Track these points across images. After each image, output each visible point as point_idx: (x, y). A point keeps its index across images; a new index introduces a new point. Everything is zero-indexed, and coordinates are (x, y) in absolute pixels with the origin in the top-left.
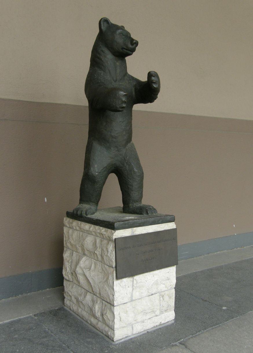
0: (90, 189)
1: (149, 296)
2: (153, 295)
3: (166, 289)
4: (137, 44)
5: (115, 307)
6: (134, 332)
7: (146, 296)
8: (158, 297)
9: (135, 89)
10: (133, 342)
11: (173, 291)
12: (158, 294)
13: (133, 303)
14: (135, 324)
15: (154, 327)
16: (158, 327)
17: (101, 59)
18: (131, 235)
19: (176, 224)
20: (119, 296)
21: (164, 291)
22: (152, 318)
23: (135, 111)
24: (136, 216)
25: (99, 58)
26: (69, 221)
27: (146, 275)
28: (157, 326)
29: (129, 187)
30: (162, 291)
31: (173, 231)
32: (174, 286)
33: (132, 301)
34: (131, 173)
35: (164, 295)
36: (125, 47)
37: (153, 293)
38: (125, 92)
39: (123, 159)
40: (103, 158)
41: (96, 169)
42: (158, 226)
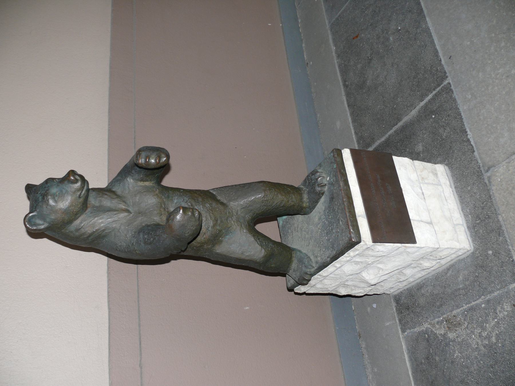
0: (277, 263)
4: (72, 172)
5: (441, 247)
6: (461, 222)
9: (142, 180)
11: (417, 163)
12: (422, 185)
15: (454, 195)
16: (454, 189)
17: (90, 235)
19: (343, 149)
25: (89, 236)
28: (453, 191)
29: (282, 205)
31: (355, 154)
32: (411, 160)
34: (266, 201)
36: (79, 193)
38: (180, 211)
39: (243, 210)
40: (240, 243)
41: (255, 251)
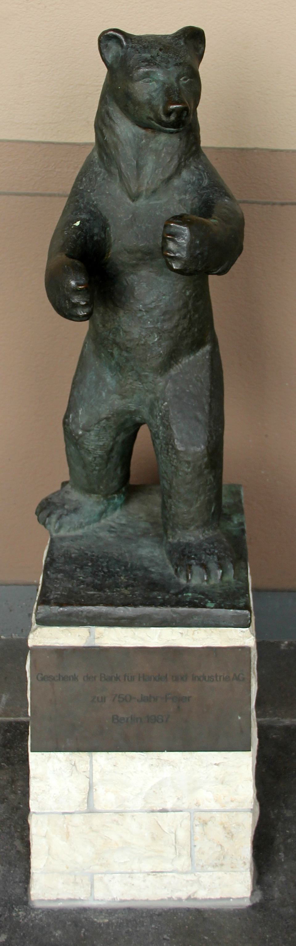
1: (153, 811)
2: (168, 813)
3: (217, 807)
7: (141, 811)
8: (187, 822)
10: (76, 923)
12: (186, 814)
13: (96, 820)
14: (103, 875)
18: (86, 645)
20: (44, 791)
21: (211, 811)
22: (162, 874)
23: (204, 147)
24: (40, 643)
26: (152, 92)
27: (133, 758)
30: (202, 807)
33: (91, 811)
35: (209, 823)
37: (169, 806)
42: (188, 630)
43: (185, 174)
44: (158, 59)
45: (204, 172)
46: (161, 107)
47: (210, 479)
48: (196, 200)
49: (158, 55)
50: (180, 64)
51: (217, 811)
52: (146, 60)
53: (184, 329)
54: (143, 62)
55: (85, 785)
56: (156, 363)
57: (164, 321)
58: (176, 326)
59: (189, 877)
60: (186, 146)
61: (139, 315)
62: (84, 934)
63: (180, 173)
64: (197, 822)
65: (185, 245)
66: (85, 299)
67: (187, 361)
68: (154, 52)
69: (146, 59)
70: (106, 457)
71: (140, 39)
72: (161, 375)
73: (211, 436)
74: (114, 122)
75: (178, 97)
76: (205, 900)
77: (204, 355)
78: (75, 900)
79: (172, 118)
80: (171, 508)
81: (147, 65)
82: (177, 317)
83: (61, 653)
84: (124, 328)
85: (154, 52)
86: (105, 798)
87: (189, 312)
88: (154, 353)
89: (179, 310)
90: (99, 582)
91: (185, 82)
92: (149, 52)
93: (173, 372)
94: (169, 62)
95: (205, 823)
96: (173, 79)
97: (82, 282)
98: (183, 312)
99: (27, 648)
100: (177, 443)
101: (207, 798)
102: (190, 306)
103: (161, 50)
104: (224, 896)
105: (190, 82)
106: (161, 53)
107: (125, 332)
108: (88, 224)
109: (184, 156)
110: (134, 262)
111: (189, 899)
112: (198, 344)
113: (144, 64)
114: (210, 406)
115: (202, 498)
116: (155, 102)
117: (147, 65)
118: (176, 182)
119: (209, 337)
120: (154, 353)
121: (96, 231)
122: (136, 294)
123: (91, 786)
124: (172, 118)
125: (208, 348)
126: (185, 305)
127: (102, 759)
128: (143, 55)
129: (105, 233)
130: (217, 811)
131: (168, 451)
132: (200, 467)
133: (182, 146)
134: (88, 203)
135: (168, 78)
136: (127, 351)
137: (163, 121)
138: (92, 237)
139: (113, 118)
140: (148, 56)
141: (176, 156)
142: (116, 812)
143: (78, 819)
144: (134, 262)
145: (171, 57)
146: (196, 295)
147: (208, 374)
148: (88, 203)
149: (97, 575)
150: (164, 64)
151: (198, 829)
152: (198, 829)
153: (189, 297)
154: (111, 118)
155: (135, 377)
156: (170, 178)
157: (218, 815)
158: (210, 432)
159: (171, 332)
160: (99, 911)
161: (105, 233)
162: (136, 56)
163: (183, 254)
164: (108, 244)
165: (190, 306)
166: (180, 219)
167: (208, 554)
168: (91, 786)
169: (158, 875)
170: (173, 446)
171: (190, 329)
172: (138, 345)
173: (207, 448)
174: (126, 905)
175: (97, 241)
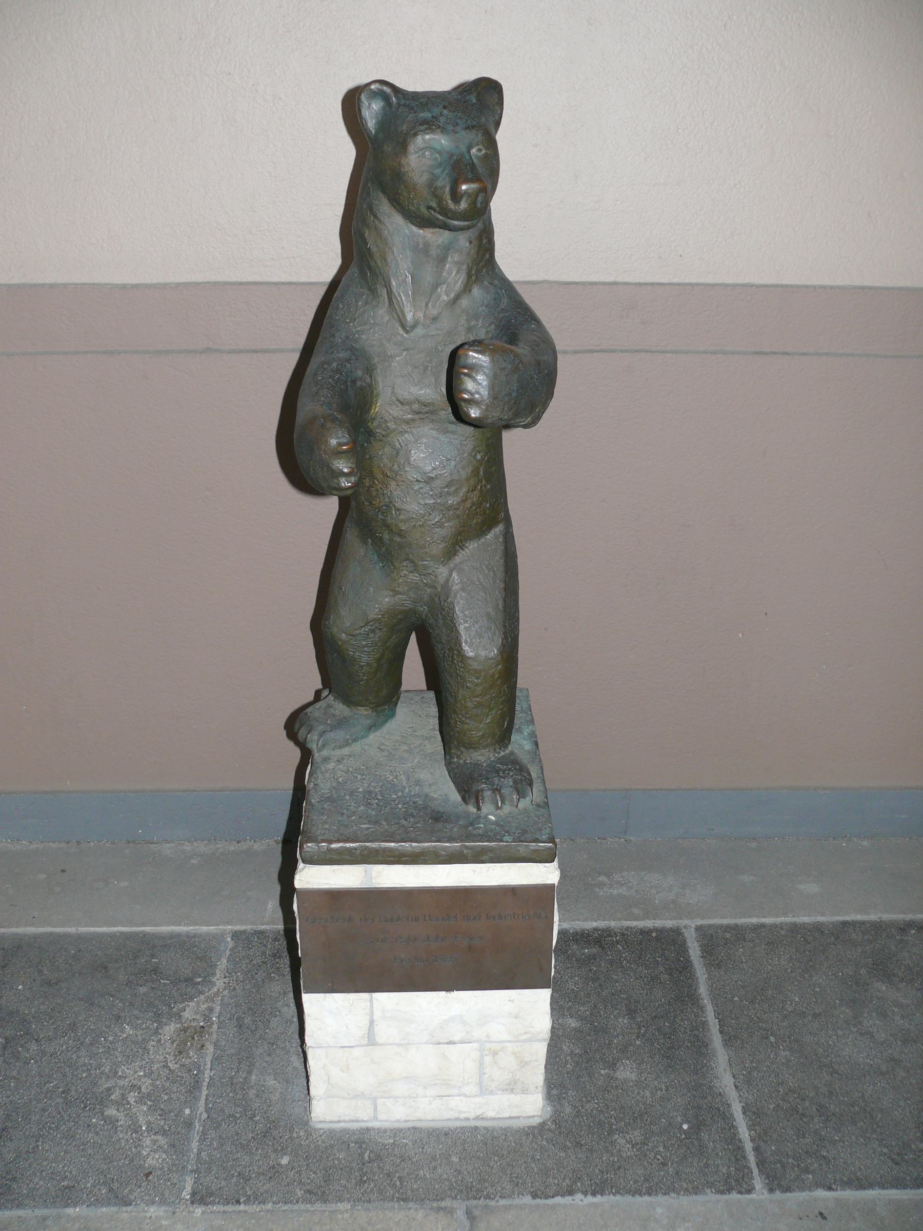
1: (439, 1044)
7: (426, 1043)
12: (476, 1045)
21: (502, 1042)
43: (476, 291)
44: (442, 119)
45: (501, 289)
46: (448, 189)
47: (504, 691)
48: (493, 327)
49: (442, 115)
50: (473, 127)
51: (509, 1041)
52: (424, 122)
53: (473, 504)
54: (420, 124)
55: (365, 1022)
56: (437, 549)
57: (448, 493)
58: (464, 501)
59: (478, 1100)
60: (478, 252)
61: (416, 488)
62: (369, 1156)
63: (470, 291)
64: (487, 1053)
65: (485, 383)
66: (350, 465)
67: (476, 545)
68: (436, 111)
69: (425, 120)
70: (375, 665)
71: (415, 96)
72: (444, 564)
73: (506, 637)
74: (380, 220)
75: (472, 172)
76: (494, 1119)
77: (496, 537)
78: (357, 1121)
79: (463, 205)
80: (456, 723)
81: (426, 129)
82: (465, 490)
83: (335, 897)
84: (396, 505)
85: (436, 111)
86: (384, 1031)
87: (480, 481)
88: (436, 536)
89: (468, 479)
90: (374, 813)
91: (480, 154)
92: (429, 111)
93: (457, 559)
94: (457, 124)
95: (495, 1054)
96: (463, 149)
97: (345, 440)
98: (472, 482)
99: (295, 889)
100: (466, 647)
101: (498, 1031)
102: (481, 473)
103: (445, 107)
104: (513, 1115)
105: (486, 156)
106: (445, 112)
107: (399, 510)
108: (348, 366)
109: (475, 267)
110: (409, 416)
111: (477, 1118)
112: (488, 524)
113: (422, 128)
114: (505, 601)
115: (494, 712)
116: (439, 183)
117: (426, 129)
118: (464, 302)
119: (502, 514)
120: (436, 536)
121: (359, 373)
122: (412, 459)
123: (372, 1022)
124: (463, 205)
125: (499, 529)
126: (476, 472)
127: (385, 1000)
128: (421, 115)
129: (371, 377)
130: (509, 1041)
131: (452, 657)
132: (493, 676)
133: (472, 252)
134: (347, 337)
135: (457, 147)
136: (400, 536)
137: (450, 210)
138: (354, 382)
139: (379, 215)
140: (427, 115)
141: (465, 267)
142: (399, 1045)
143: (357, 1052)
144: (409, 416)
145: (460, 118)
146: (488, 461)
147: (502, 561)
148: (347, 337)
149: (369, 803)
150: (450, 127)
151: (488, 1059)
152: (488, 1059)
153: (481, 461)
154: (375, 216)
155: (412, 569)
156: (457, 297)
157: (509, 1045)
158: (505, 633)
159: (458, 509)
160: (382, 1132)
161: (371, 377)
162: (411, 116)
163: (485, 393)
164: (375, 392)
165: (481, 473)
166: (478, 344)
167: (502, 777)
168: (372, 1022)
169: (445, 1098)
170: (459, 652)
171: (481, 504)
172: (414, 526)
173: (501, 653)
174: (410, 1125)
175: (361, 388)
